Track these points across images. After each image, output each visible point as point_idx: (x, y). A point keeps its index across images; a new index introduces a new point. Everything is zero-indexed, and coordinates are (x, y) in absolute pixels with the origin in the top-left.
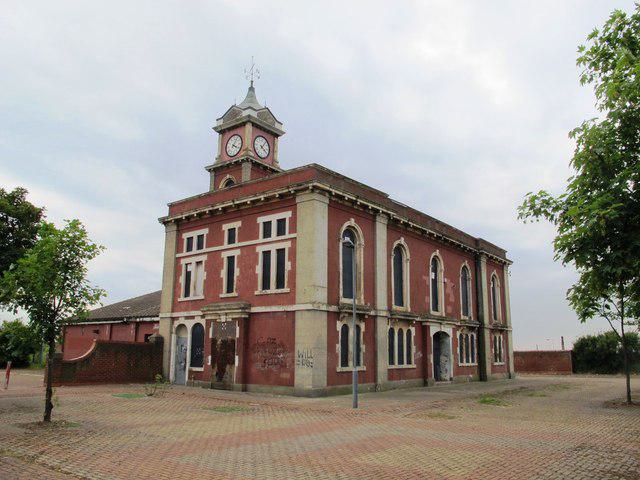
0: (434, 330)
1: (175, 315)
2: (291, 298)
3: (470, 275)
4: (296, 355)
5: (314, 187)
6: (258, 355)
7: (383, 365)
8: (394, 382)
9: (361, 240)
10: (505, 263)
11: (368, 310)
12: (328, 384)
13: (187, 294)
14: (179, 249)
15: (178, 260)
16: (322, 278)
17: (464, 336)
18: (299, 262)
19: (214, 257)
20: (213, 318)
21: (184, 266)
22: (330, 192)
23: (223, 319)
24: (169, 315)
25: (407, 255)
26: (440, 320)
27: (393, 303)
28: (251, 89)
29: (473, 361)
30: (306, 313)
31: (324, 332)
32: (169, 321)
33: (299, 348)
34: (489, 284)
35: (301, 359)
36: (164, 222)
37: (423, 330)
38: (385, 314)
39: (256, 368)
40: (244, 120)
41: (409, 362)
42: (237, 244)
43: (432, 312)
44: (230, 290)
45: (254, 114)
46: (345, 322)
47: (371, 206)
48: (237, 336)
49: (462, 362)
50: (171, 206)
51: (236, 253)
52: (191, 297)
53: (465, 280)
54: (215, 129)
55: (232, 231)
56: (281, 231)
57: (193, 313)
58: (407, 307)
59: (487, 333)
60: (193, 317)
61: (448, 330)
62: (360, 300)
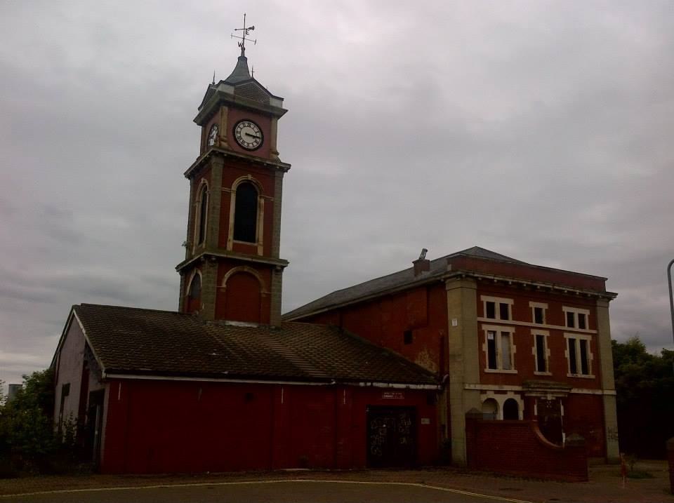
1: (485, 387)
20: (539, 395)
23: (549, 397)
28: (242, 59)
35: (611, 434)
42: (544, 325)
48: (562, 414)
51: (546, 334)
57: (506, 388)
60: (505, 392)
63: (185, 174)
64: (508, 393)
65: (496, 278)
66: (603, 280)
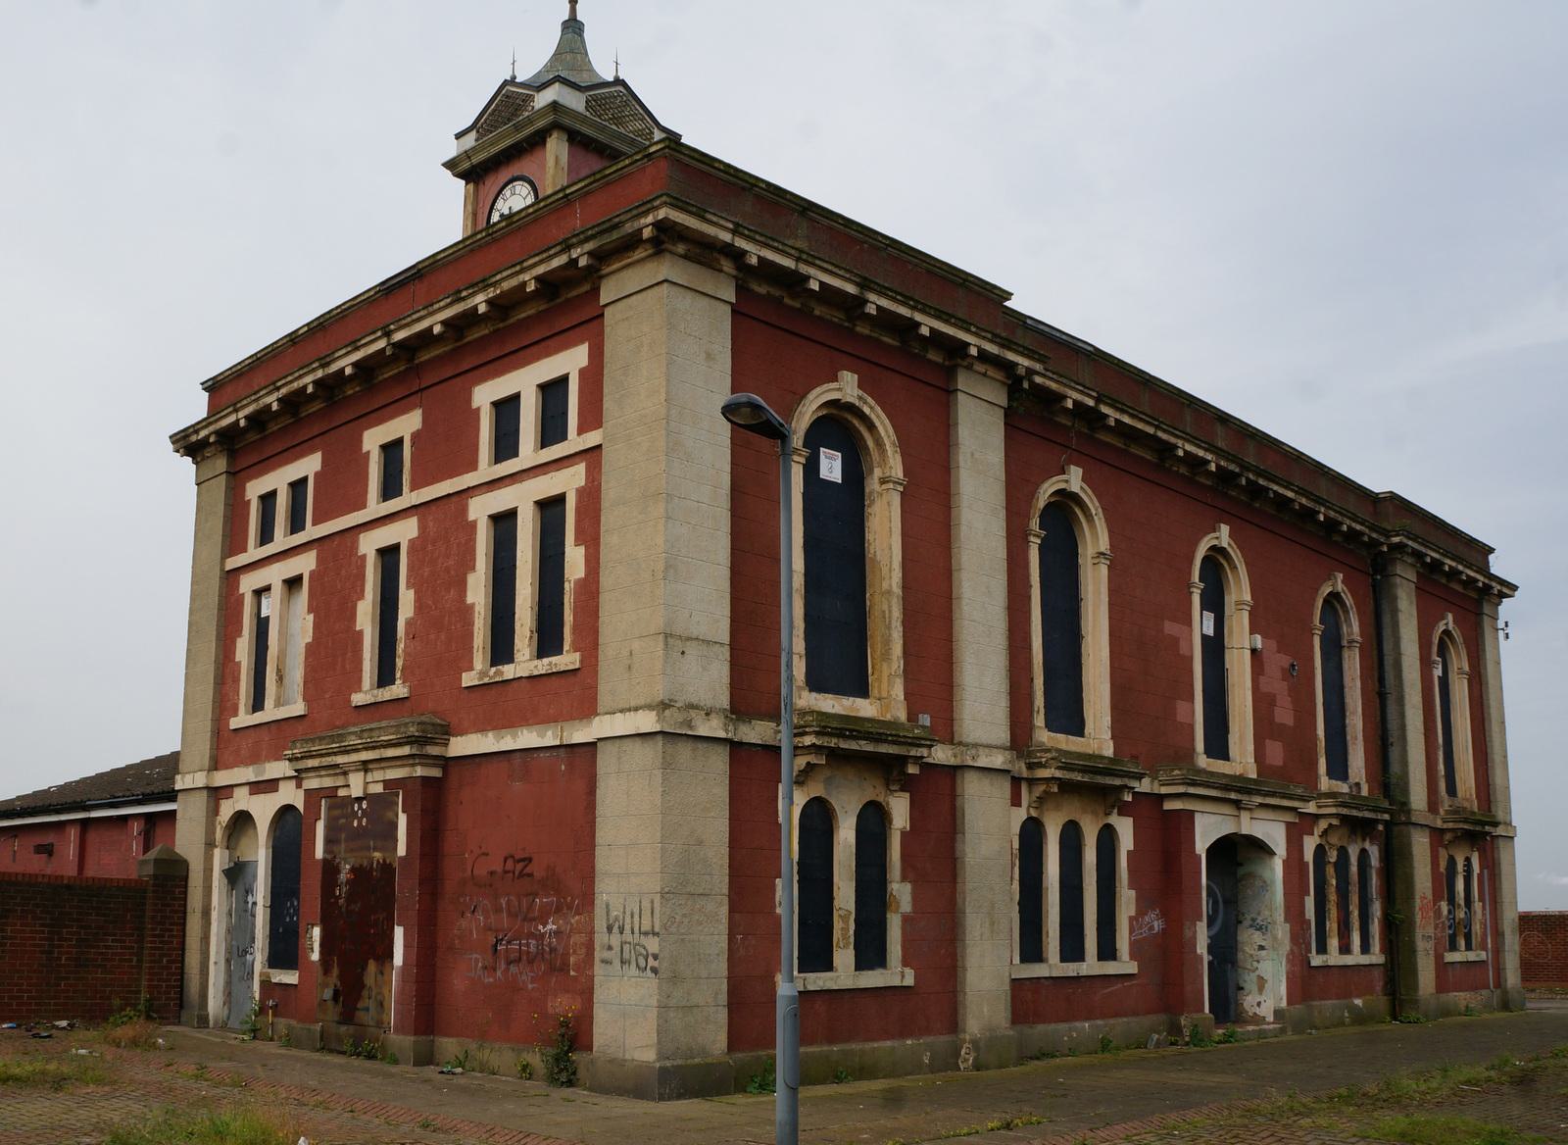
0: (1208, 828)
1: (222, 778)
2: (578, 694)
3: (1353, 627)
4: (600, 924)
5: (661, 226)
6: (470, 925)
7: (989, 965)
8: (1042, 1031)
9: (889, 464)
10: (1487, 588)
11: (916, 743)
12: (732, 1046)
13: (258, 704)
14: (234, 542)
15: (231, 577)
16: (708, 604)
17: (1333, 856)
18: (609, 540)
19: (337, 550)
20: (328, 782)
21: (248, 600)
22: (738, 256)
24: (200, 779)
25: (1095, 539)
26: (1235, 793)
27: (1039, 720)
28: (573, 27)
29: (1365, 949)
30: (638, 743)
31: (717, 829)
32: (200, 801)
33: (609, 894)
34: (1426, 664)
35: (615, 940)
36: (188, 443)
37: (1166, 832)
38: (998, 760)
39: (465, 975)
40: (541, 124)
41: (1107, 952)
42: (409, 498)
43: (1203, 761)
44: (385, 678)
45: (576, 102)
46: (816, 789)
47: (927, 324)
49: (1322, 949)
50: (213, 387)
52: (270, 713)
53: (1333, 648)
54: (450, 165)
55: (391, 449)
56: (552, 429)
58: (1099, 736)
59: (1420, 845)
61: (1272, 831)
62: (885, 700)
63: (170, 437)
64: (282, 784)
65: (241, 414)
66: (681, 136)
